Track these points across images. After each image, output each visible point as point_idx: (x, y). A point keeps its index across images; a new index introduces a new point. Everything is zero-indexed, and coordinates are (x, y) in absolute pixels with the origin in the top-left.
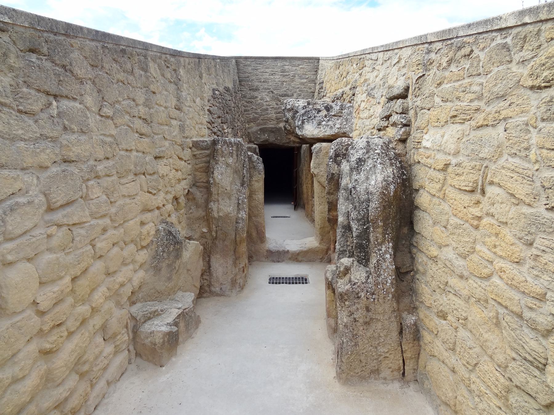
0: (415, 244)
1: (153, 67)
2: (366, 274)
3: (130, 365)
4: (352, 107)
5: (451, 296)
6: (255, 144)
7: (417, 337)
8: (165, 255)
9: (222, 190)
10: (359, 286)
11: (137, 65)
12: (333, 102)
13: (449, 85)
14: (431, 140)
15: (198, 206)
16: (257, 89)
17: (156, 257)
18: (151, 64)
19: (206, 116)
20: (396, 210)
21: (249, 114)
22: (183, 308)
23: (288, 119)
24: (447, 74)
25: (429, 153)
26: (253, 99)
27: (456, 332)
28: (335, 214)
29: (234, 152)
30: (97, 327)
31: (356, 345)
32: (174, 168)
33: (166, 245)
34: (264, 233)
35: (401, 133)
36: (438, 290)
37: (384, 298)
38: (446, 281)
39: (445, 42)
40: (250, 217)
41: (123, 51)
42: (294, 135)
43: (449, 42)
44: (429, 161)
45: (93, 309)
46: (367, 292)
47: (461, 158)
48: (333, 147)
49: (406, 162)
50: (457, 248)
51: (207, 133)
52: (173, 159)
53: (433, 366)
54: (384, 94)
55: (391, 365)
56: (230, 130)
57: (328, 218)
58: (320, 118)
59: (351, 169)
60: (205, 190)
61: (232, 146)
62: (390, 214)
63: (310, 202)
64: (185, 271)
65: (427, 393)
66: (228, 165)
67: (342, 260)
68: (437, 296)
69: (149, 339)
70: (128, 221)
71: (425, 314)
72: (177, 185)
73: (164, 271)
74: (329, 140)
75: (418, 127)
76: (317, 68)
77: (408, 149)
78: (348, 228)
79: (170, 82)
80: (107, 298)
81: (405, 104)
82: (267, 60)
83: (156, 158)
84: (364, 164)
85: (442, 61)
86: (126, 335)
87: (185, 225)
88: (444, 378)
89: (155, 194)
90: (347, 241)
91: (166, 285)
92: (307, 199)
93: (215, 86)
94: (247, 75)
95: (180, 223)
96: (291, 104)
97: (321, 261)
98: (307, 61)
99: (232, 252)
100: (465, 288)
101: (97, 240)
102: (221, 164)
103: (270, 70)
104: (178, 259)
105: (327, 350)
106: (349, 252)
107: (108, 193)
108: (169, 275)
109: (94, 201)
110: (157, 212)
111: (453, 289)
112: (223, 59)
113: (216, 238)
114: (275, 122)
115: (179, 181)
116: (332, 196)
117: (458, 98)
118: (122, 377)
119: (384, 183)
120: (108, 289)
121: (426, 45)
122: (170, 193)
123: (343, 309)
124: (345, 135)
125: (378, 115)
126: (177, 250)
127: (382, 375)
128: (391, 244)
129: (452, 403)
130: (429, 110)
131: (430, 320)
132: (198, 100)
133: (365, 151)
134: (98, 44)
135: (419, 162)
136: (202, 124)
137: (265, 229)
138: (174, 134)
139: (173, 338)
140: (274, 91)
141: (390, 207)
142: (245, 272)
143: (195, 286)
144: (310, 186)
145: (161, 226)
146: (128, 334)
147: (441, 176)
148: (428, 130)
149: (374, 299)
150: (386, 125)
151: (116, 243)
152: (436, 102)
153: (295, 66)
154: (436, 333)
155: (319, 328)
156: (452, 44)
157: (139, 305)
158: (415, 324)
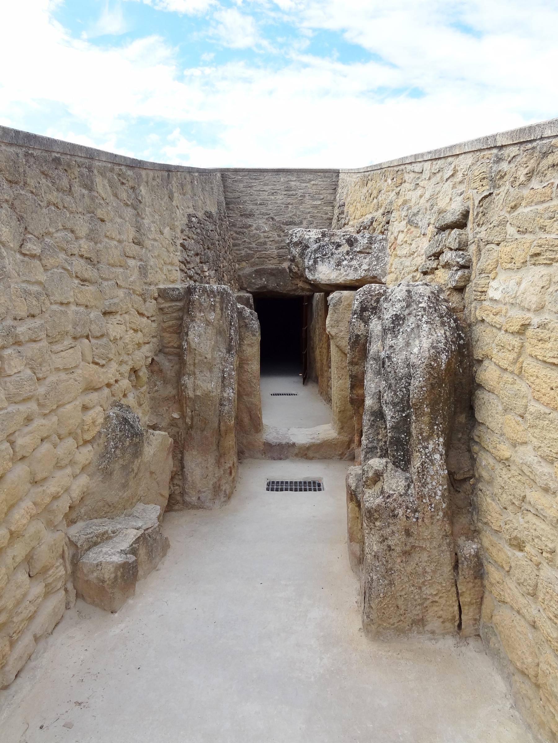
0: (476, 439)
1: (101, 185)
2: (406, 481)
3: (68, 611)
4: (386, 240)
5: (530, 517)
6: (248, 292)
7: (479, 572)
8: (118, 452)
9: (200, 358)
10: (395, 500)
11: (77, 180)
12: (358, 233)
13: (529, 209)
14: (501, 289)
15: (165, 381)
16: (250, 215)
17: (106, 455)
18: (98, 180)
19: (179, 254)
20: (450, 390)
21: (239, 250)
22: (145, 527)
23: (294, 257)
24: (526, 192)
25: (497, 307)
26: (247, 228)
27: (538, 569)
28: (360, 392)
29: (218, 305)
30: (18, 560)
31: (391, 583)
32: (131, 328)
33: (120, 438)
34: (260, 419)
35: (457, 278)
36: (510, 508)
37: (432, 517)
38: (523, 495)
39: (524, 145)
40: (240, 395)
41: (57, 161)
42: (302, 279)
43: (530, 146)
44: (498, 319)
45: (12, 533)
46: (407, 508)
47: (546, 317)
48: (358, 297)
49: (464, 320)
50: (540, 447)
51: (179, 277)
52: (130, 314)
53: (503, 617)
54: (432, 222)
55: (441, 612)
56: (212, 273)
57: (351, 398)
58: (340, 256)
59: (385, 331)
60: (176, 358)
61: (215, 297)
62: (440, 396)
63: (326, 374)
64: (148, 475)
65: (495, 655)
66: (208, 323)
67: (371, 462)
68: (510, 515)
69: (95, 574)
70: (63, 405)
71: (491, 541)
72: (136, 352)
73: (117, 476)
74: (352, 286)
75: (482, 270)
76: (336, 185)
77: (467, 301)
78: (379, 415)
79: (127, 205)
80: (32, 517)
81: (463, 236)
83: (105, 314)
84: (403, 323)
85: (519, 173)
86: (62, 568)
87: (147, 408)
88: (520, 636)
89: (103, 366)
90: (378, 434)
91: (121, 494)
92: (322, 370)
93: (191, 211)
94: (237, 194)
95: (140, 405)
96: (298, 235)
97: (341, 459)
98: (322, 174)
99: (215, 447)
100: (552, 507)
101: (17, 434)
102: (199, 322)
103: (270, 187)
104: (137, 457)
105: (350, 588)
106: (382, 450)
107: (33, 365)
108: (123, 481)
109: (13, 378)
110: (106, 391)
111: (534, 507)
112: (205, 174)
113: (191, 427)
114: (276, 261)
115: (139, 345)
116: (356, 367)
117: (543, 228)
118: (55, 630)
119: (432, 351)
120: (35, 504)
121: (495, 151)
122: (126, 363)
123: (373, 532)
124: (375, 280)
125: (423, 252)
126: (136, 445)
127: (429, 627)
128: (441, 440)
129: (531, 672)
130: (498, 244)
131: (499, 550)
132: (167, 230)
133: (404, 304)
134: (18, 151)
135: (483, 321)
136: (172, 264)
137: (261, 413)
138: (131, 279)
139: (129, 572)
140: (276, 218)
141: (440, 386)
142: (233, 474)
143: (162, 495)
144: (325, 351)
145: (113, 411)
146: (65, 567)
147: (515, 341)
148: (497, 274)
149: (417, 518)
150: (434, 266)
151: (46, 438)
152: (509, 233)
153: (304, 181)
154: (507, 569)
155: (337, 557)
156: (534, 148)
157: (80, 524)
158: (477, 555)
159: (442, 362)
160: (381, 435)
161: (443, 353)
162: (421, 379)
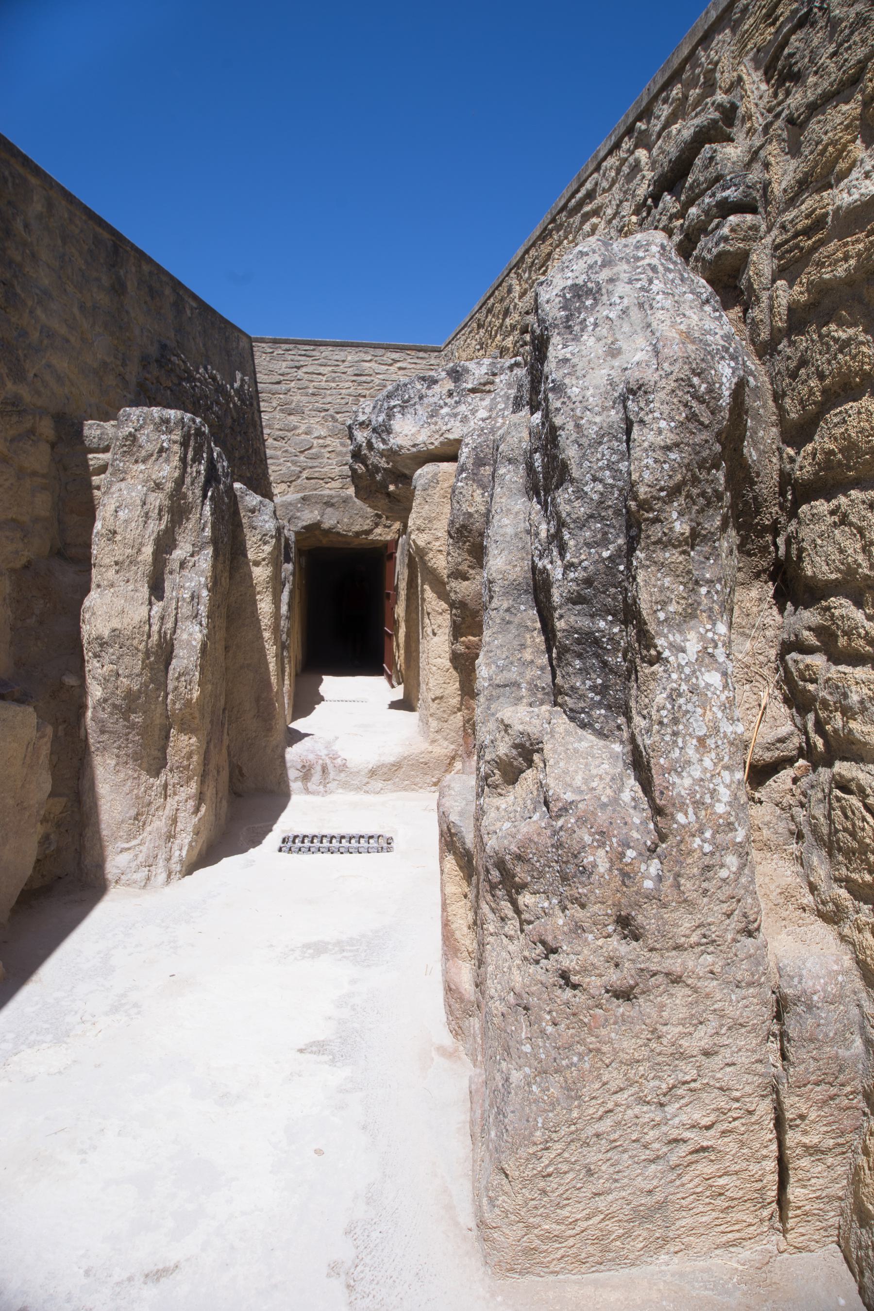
58: (435, 399)
82: (322, 348)
159: (721, 384)
160: (529, 650)
161: (723, 358)
162: (663, 424)
